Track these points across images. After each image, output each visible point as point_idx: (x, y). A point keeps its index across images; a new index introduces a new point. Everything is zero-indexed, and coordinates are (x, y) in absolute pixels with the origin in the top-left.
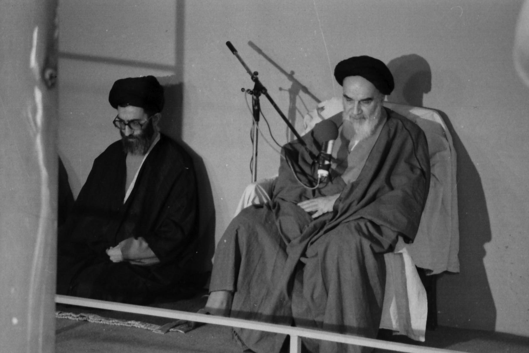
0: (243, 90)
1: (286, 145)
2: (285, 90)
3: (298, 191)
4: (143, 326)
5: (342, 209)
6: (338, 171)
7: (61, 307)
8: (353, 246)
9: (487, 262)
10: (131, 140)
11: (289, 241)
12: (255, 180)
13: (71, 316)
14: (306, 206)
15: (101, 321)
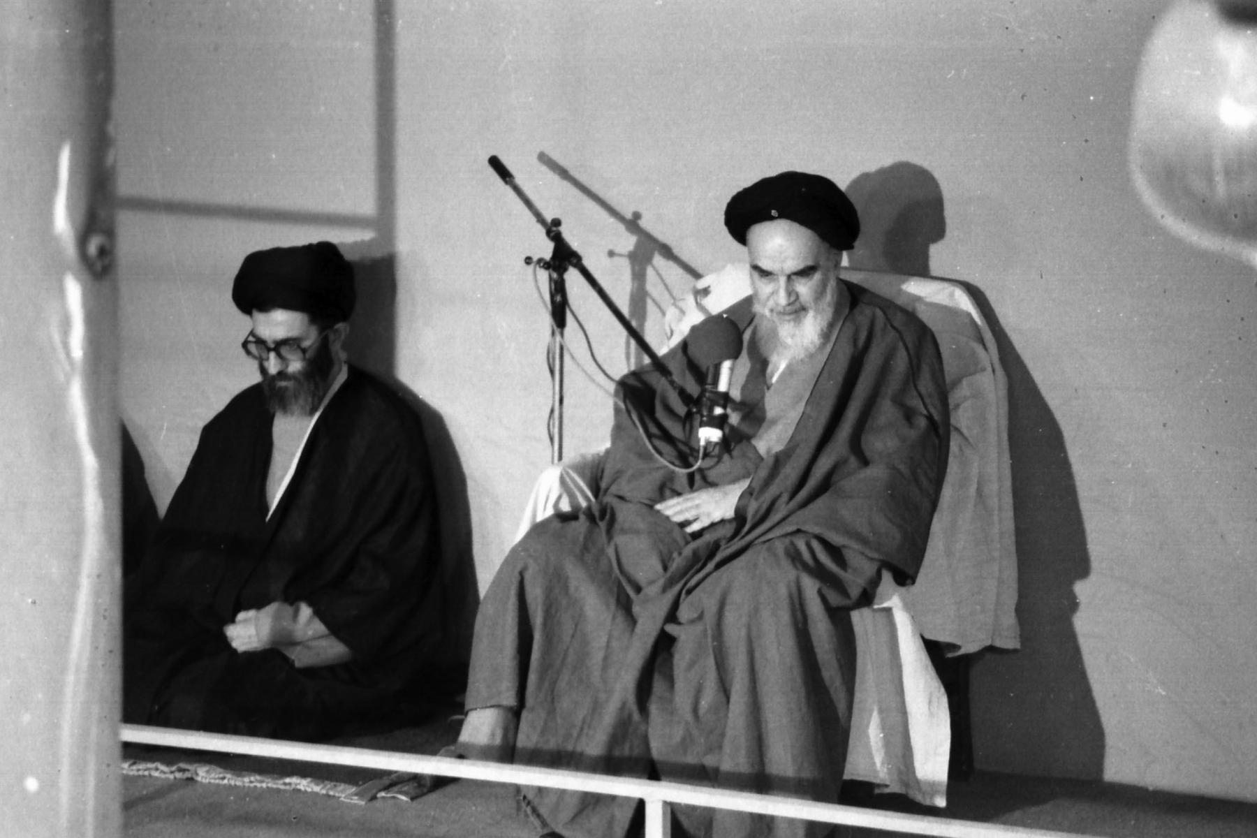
0: (528, 260)
1: (626, 377)
2: (621, 255)
3: (657, 476)
4: (317, 789)
5: (757, 512)
6: (745, 428)
7: (133, 752)
8: (783, 591)
9: (1082, 623)
10: (283, 384)
11: (638, 589)
12: (560, 458)
13: (157, 769)
14: (674, 509)
15: (223, 778)
